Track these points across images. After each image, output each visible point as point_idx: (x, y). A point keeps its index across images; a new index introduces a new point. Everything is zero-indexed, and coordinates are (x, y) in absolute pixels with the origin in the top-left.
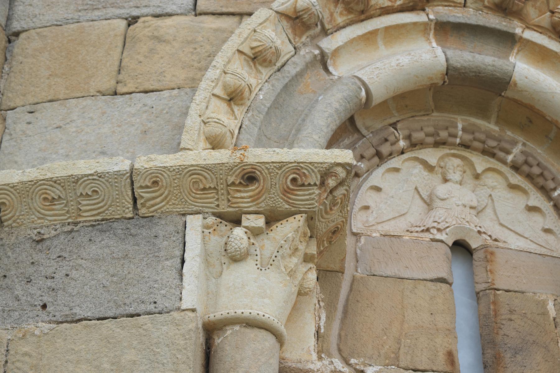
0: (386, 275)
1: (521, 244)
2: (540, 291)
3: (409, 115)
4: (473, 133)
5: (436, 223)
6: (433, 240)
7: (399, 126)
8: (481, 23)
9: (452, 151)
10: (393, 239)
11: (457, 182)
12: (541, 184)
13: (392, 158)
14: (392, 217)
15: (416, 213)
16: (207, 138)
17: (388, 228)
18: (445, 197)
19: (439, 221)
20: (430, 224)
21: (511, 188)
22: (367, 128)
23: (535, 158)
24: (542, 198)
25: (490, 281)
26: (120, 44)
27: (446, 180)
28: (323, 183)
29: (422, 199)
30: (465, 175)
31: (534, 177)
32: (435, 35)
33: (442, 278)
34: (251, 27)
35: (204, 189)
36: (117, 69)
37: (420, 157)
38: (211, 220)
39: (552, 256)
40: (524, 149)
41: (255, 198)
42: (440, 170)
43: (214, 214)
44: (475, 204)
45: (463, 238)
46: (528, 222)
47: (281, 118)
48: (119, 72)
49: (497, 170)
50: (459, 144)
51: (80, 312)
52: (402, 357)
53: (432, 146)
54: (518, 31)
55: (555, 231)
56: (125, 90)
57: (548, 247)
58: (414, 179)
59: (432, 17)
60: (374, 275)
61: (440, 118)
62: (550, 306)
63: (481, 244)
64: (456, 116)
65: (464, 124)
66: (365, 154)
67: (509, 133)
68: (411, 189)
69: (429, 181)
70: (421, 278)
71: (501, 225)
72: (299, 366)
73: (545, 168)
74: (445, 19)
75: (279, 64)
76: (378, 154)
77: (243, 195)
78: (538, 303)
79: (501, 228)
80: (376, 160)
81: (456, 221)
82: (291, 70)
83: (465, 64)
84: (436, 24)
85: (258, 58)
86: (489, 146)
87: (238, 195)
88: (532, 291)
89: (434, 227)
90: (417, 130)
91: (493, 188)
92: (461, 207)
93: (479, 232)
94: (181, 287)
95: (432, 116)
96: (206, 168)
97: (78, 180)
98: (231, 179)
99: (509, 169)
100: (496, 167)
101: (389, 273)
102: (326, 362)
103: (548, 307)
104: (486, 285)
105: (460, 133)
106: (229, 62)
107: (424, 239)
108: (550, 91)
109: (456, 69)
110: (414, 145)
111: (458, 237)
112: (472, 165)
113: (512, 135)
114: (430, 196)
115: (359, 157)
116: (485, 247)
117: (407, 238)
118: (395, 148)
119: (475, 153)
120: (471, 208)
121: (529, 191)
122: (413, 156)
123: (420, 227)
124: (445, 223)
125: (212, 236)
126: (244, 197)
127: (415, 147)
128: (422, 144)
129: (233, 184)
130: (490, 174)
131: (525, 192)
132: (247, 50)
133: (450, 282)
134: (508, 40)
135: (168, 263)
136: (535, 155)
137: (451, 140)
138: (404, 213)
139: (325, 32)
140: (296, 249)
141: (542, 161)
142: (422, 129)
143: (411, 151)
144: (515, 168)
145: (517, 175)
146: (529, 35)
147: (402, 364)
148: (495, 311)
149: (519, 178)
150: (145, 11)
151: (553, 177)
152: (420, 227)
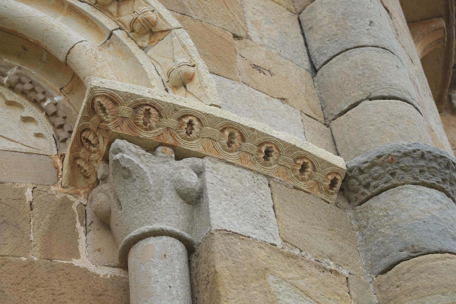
2: (20, 181)
12: (33, 98)
21: (8, 105)
23: (28, 78)
24: (37, 111)
39: (38, 154)
40: (19, 71)
46: (19, 129)
55: (45, 134)
57: (36, 148)
62: (29, 195)
67: (6, 60)
73: (38, 85)
88: (12, 181)
99: (7, 89)
103: (25, 194)
108: (27, 16)
113: (9, 62)
121: (25, 106)
131: (21, 107)
136: (28, 75)
141: (35, 80)
144: (12, 87)
145: (14, 94)
149: (16, 96)
151: (30, 81)
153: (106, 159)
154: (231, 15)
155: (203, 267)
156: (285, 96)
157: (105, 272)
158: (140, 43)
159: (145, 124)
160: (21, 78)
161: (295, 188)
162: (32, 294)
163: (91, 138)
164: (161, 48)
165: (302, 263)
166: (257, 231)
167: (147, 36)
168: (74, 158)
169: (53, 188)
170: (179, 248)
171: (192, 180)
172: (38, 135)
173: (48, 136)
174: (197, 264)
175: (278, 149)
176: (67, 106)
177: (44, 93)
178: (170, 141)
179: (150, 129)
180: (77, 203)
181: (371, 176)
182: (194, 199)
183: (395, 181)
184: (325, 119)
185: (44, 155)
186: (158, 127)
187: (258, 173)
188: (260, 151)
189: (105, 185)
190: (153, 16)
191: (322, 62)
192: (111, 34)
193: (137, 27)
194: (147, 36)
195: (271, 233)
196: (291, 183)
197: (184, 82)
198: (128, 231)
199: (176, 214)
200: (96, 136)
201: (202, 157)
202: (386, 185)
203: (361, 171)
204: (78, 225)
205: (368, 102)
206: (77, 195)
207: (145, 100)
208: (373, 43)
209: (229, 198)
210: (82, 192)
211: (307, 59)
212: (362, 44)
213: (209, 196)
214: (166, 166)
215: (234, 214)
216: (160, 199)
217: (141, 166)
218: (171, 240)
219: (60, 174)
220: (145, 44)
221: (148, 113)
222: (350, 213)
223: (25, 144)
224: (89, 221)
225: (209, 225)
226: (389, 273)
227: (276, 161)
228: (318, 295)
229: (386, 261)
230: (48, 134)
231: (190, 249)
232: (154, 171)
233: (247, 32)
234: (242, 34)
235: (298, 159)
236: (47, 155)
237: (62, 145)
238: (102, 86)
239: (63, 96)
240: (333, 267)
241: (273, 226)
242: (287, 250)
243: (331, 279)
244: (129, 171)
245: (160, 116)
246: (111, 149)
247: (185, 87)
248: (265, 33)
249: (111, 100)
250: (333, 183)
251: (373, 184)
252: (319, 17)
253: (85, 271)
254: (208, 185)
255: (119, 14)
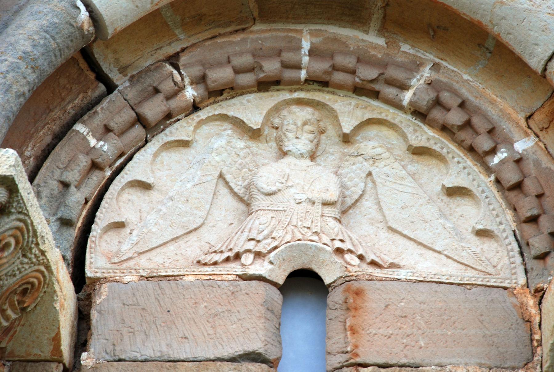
0: (143, 358)
1: (427, 266)
2: (453, 361)
3: (207, 35)
4: (332, 57)
5: (253, 243)
7: (183, 60)
9: (296, 95)
10: (163, 283)
11: (302, 155)
12: (468, 142)
13: (175, 122)
14: (170, 238)
17: (146, 264)
18: (274, 189)
19: (260, 237)
20: (240, 245)
22: (123, 70)
23: (455, 93)
24: (475, 168)
25: (349, 349)
27: (284, 154)
29: (235, 194)
30: (323, 137)
31: (455, 130)
33: (254, 352)
37: (231, 113)
39: (486, 286)
40: (435, 76)
42: (274, 133)
44: (333, 195)
45: (307, 266)
46: (442, 221)
49: (386, 121)
50: (306, 81)
53: (256, 89)
58: (217, 159)
60: (120, 360)
61: (267, 35)
63: (339, 275)
64: (298, 27)
65: (314, 40)
66: (112, 125)
67: (405, 48)
68: (209, 178)
69: (247, 160)
70: (212, 357)
73: (478, 111)
76: (140, 120)
79: (390, 235)
81: (293, 233)
86: (363, 80)
88: (437, 361)
89: (249, 251)
90: (219, 65)
91: (375, 159)
92: (305, 206)
93: (339, 251)
95: (251, 32)
99: (409, 117)
100: (383, 116)
101: (149, 353)
105: (306, 60)
107: (224, 277)
110: (217, 93)
111: (297, 266)
113: (412, 51)
114: (248, 188)
115: (101, 130)
116: (347, 280)
117: (191, 278)
118: (174, 104)
119: (342, 93)
120: (325, 204)
122: (216, 113)
123: (222, 252)
124: (270, 240)
127: (221, 94)
128: (232, 88)
133: (272, 358)
136: (456, 86)
137: (289, 74)
138: (195, 226)
141: (471, 98)
142: (229, 62)
143: (213, 103)
144: (420, 114)
145: (426, 128)
149: (430, 132)
151: (490, 127)
152: (222, 252)
160: (441, 95)
173: (505, 235)
176: (544, 166)
177: (491, 132)
185: (498, 287)
219: (537, 337)
223: (456, 258)
230: (504, 230)
236: (505, 288)
239: (533, 137)
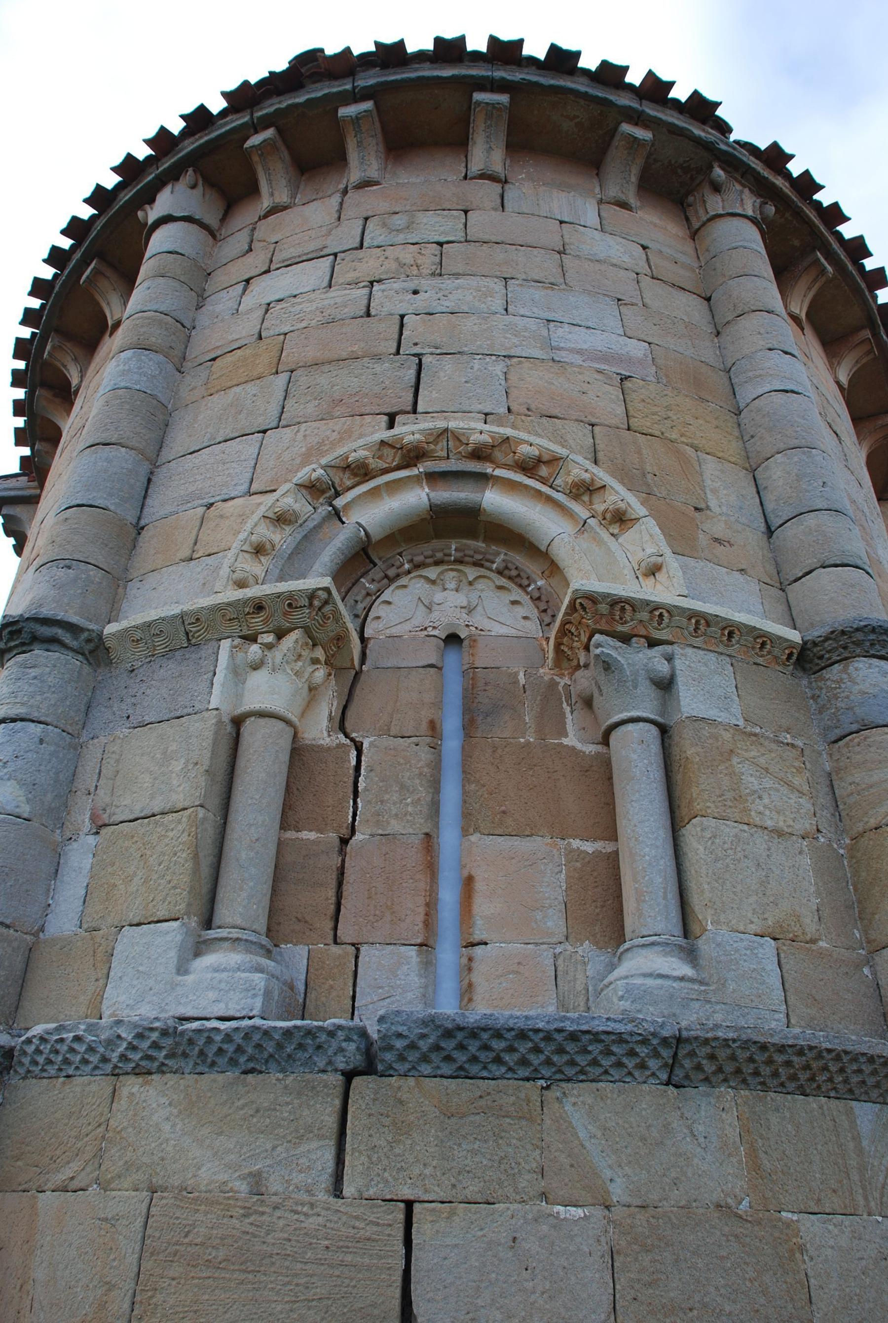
1: (503, 630)
6: (427, 636)
7: (404, 553)
8: (459, 469)
15: (420, 618)
16: (235, 583)
17: (395, 631)
22: (380, 559)
26: (198, 524)
27: (445, 589)
28: (311, 605)
32: (427, 483)
34: (275, 498)
35: (230, 620)
36: (193, 541)
38: (238, 641)
40: (505, 557)
41: (265, 622)
43: (240, 637)
44: (465, 604)
47: (296, 560)
48: (195, 543)
50: (454, 561)
51: (147, 719)
52: (392, 728)
54: (489, 471)
56: (197, 556)
59: (421, 470)
62: (521, 676)
67: (494, 547)
71: (489, 618)
72: (314, 742)
73: (523, 570)
74: (431, 471)
75: (300, 522)
76: (386, 576)
77: (257, 620)
78: (510, 675)
80: (386, 581)
82: (311, 524)
83: (444, 501)
84: (426, 474)
85: (281, 519)
87: (254, 621)
91: (482, 590)
93: (467, 626)
94: (211, 693)
96: (229, 604)
97: (149, 626)
98: (247, 610)
101: (389, 665)
102: (333, 738)
104: (468, 666)
106: (256, 525)
109: (437, 505)
110: (418, 566)
112: (466, 575)
116: (470, 636)
118: (400, 570)
120: (462, 608)
125: (238, 653)
126: (257, 621)
129: (248, 613)
130: (481, 580)
132: (271, 515)
134: (483, 478)
135: (206, 677)
137: (446, 558)
139: (337, 494)
140: (300, 656)
144: (500, 573)
146: (498, 472)
147: (392, 734)
148: (473, 684)
149: (504, 580)
150: (218, 498)
153: (587, 648)
154: (692, 487)
155: (675, 751)
156: (743, 567)
157: (590, 749)
158: (611, 531)
159: (621, 619)
161: (755, 664)
162: (531, 773)
163: (573, 630)
164: (630, 536)
165: (762, 740)
166: (722, 714)
167: (618, 524)
168: (558, 645)
169: (541, 671)
170: (654, 730)
171: (663, 668)
172: (525, 618)
174: (670, 745)
175: (739, 630)
177: (528, 578)
178: (643, 632)
179: (625, 623)
180: (562, 684)
181: (824, 649)
182: (665, 685)
183: (846, 655)
184: (781, 583)
186: (632, 620)
187: (722, 654)
188: (723, 634)
189: (586, 671)
190: (622, 505)
191: (778, 525)
192: (585, 522)
193: (608, 516)
194: (618, 524)
195: (733, 715)
196: (752, 660)
197: (653, 571)
198: (609, 716)
199: (651, 701)
200: (577, 629)
201: (671, 643)
202: (839, 658)
203: (815, 644)
204: (565, 705)
205: (823, 570)
206: (562, 676)
207: (620, 598)
208: (826, 507)
209: (696, 683)
210: (566, 673)
211: (763, 521)
212: (815, 508)
213: (679, 683)
214: (641, 655)
215: (702, 699)
216: (635, 687)
217: (619, 658)
218: (648, 726)
220: (616, 531)
221: (623, 609)
222: (805, 682)
224: (573, 701)
225: (680, 711)
226: (841, 743)
227: (738, 642)
228: (777, 770)
229: (838, 732)
231: (664, 730)
232: (630, 662)
233: (706, 503)
234: (703, 506)
235: (758, 637)
237: (547, 628)
238: (583, 588)
240: (789, 741)
241: (736, 708)
242: (749, 729)
243: (790, 754)
244: (608, 664)
245: (634, 610)
246: (592, 643)
247: (654, 575)
248: (723, 501)
249: (590, 600)
250: (790, 655)
251: (827, 656)
252: (775, 477)
253: (573, 748)
254: (678, 672)
255: (591, 503)
